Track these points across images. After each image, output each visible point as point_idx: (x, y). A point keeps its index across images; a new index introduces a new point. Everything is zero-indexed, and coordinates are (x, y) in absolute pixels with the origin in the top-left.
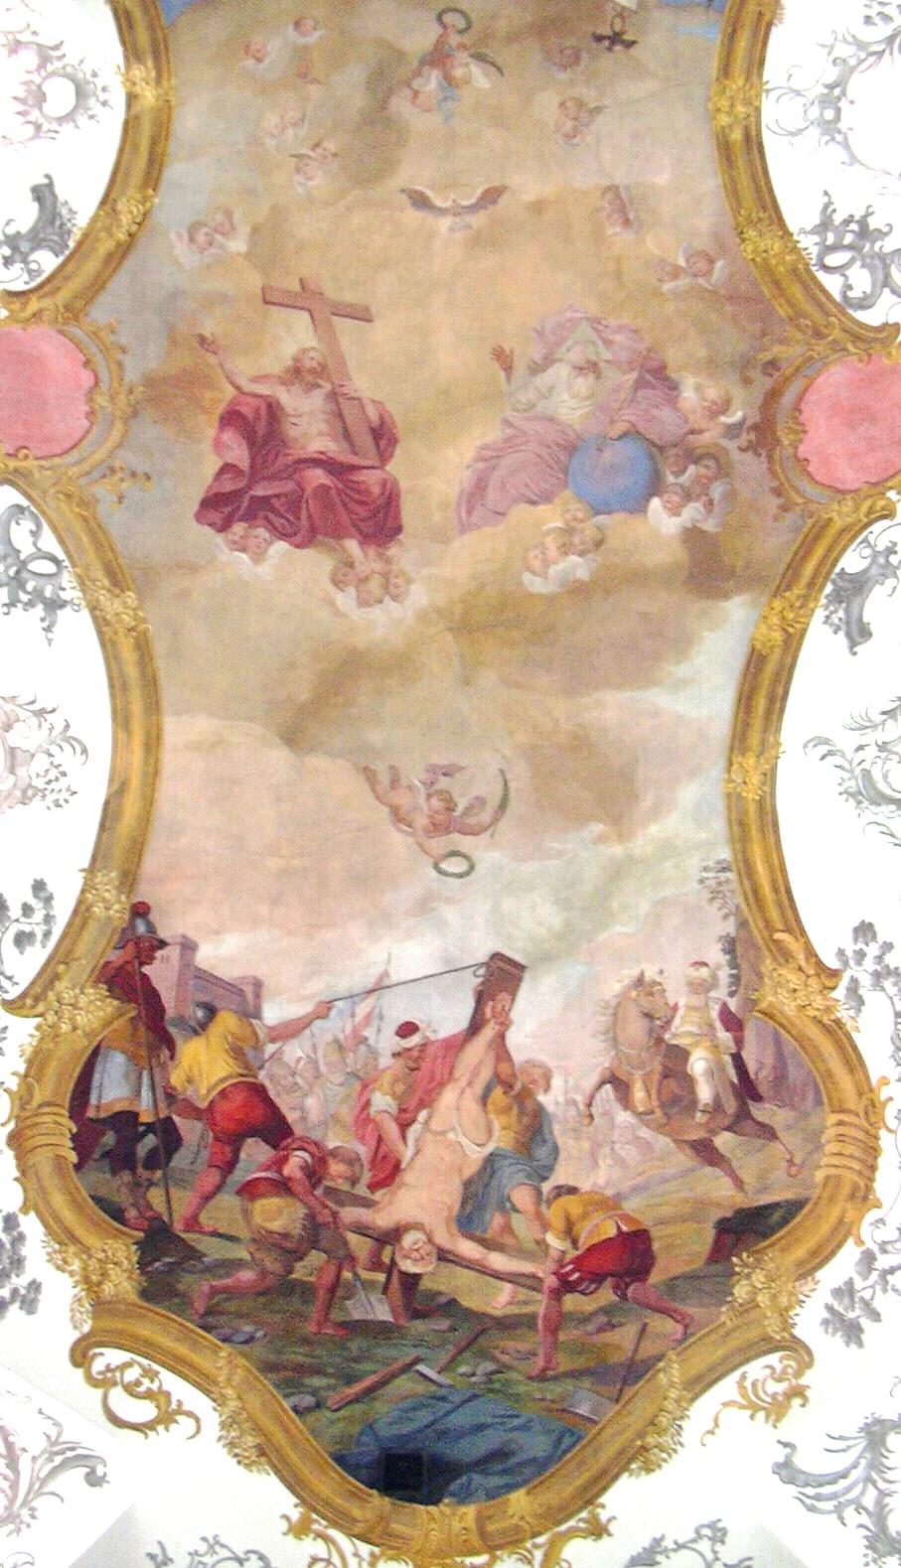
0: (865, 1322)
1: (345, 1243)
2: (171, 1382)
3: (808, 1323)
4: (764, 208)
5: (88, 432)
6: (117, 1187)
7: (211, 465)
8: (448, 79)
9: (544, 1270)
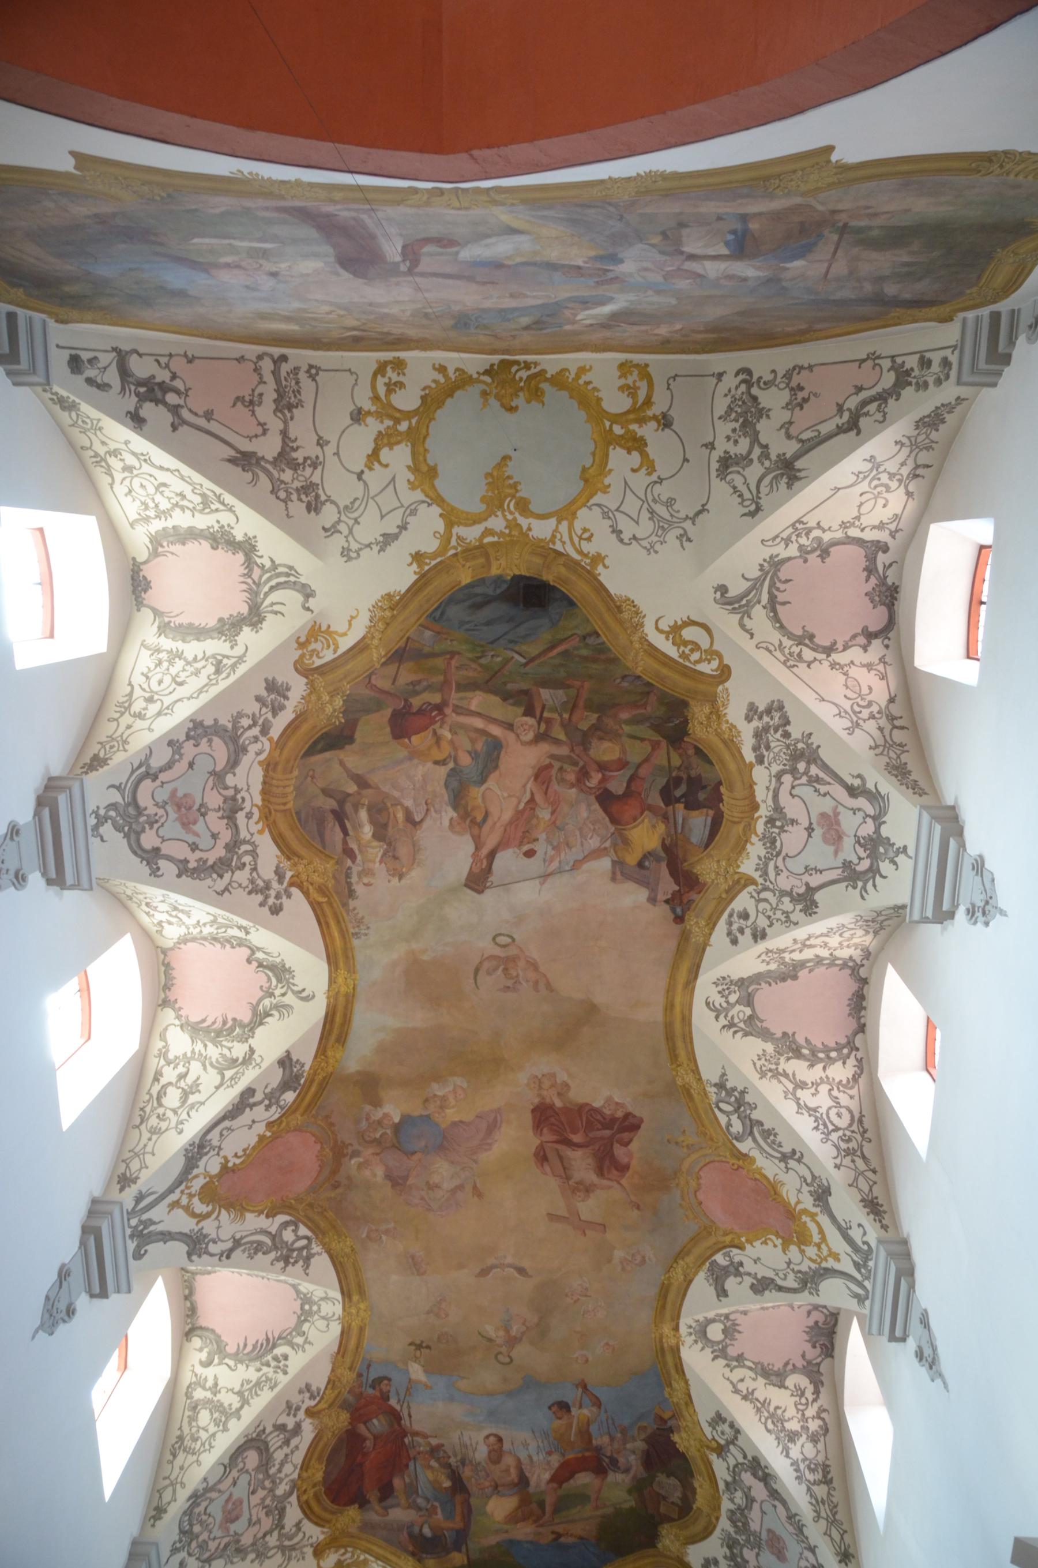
0: (264, 693)
1: (566, 734)
2: (671, 651)
3: (298, 687)
4: (340, 1263)
5: (701, 1169)
6: (698, 768)
7: (634, 1146)
8: (507, 1330)
9: (453, 717)
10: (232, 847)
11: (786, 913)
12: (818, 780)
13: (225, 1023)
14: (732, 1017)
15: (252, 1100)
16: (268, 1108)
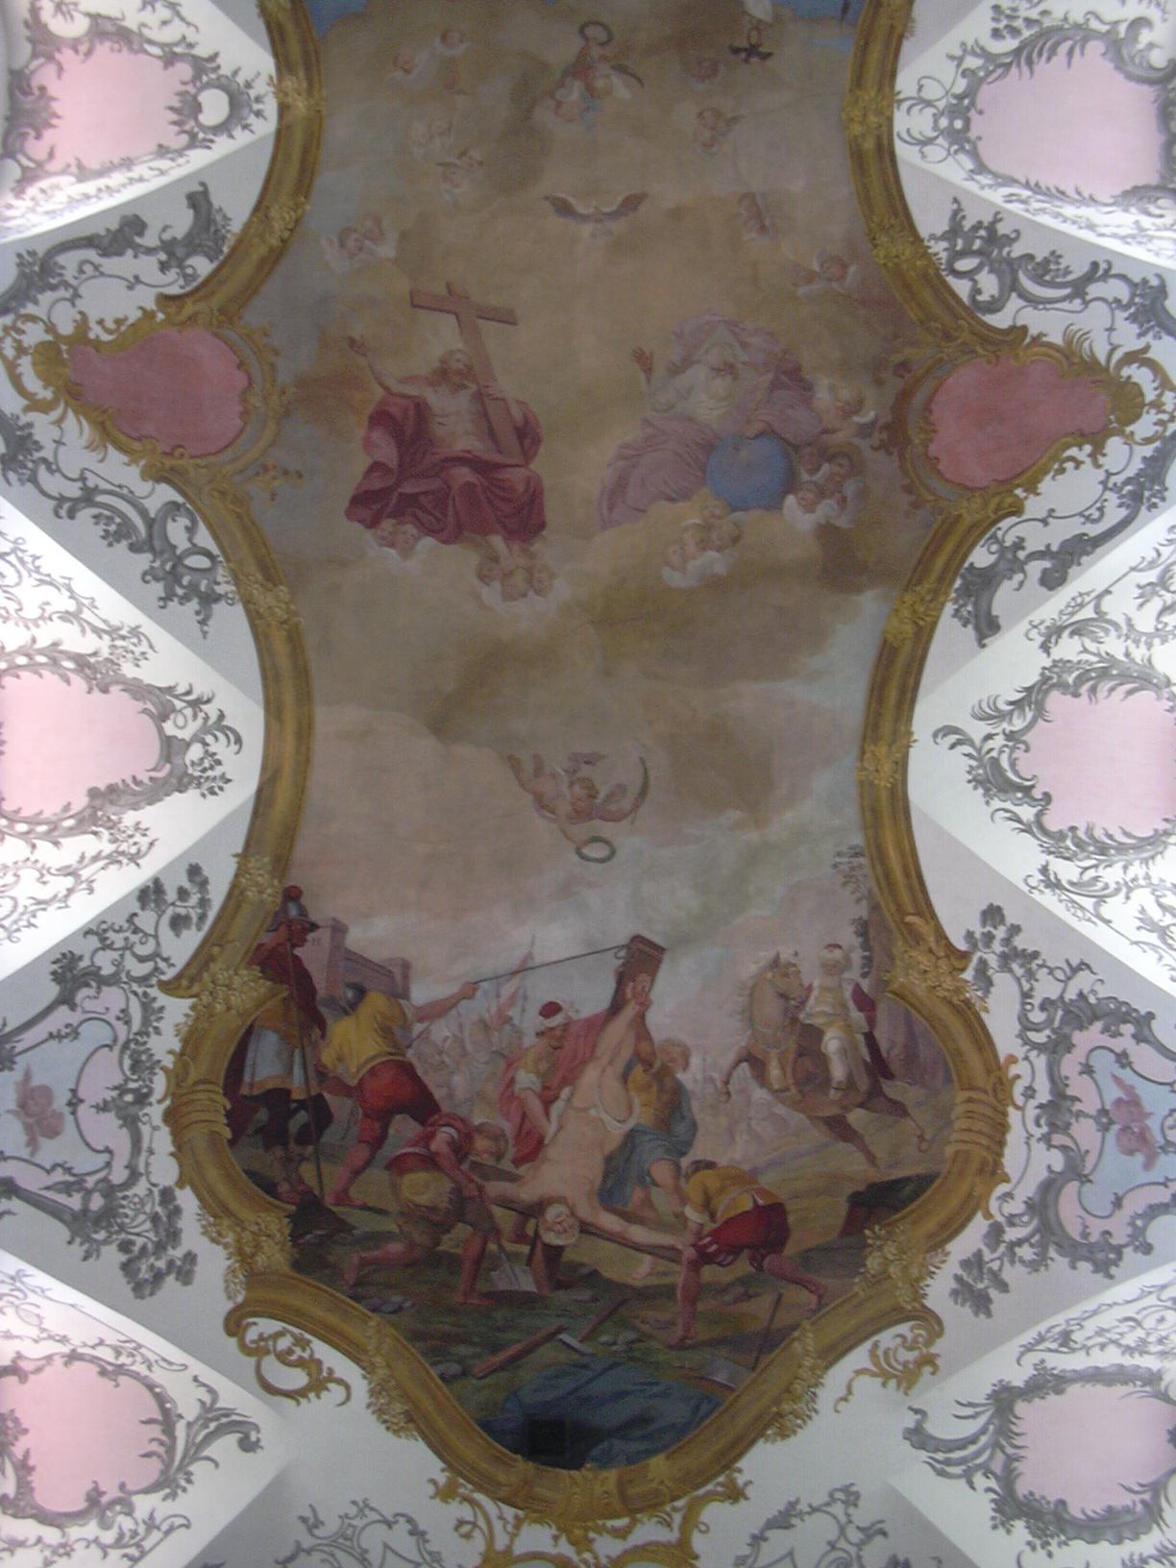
0: (993, 1293)
1: (491, 1216)
3: (938, 1292)
4: (896, 215)
5: (241, 431)
6: (270, 1162)
7: (361, 463)
8: (590, 90)
9: (682, 1242)
10: (1059, 1046)
11: (106, 945)
12: (67, 1188)
13: (1093, 690)
14: (195, 716)
15: (1047, 564)
16: (1019, 544)
